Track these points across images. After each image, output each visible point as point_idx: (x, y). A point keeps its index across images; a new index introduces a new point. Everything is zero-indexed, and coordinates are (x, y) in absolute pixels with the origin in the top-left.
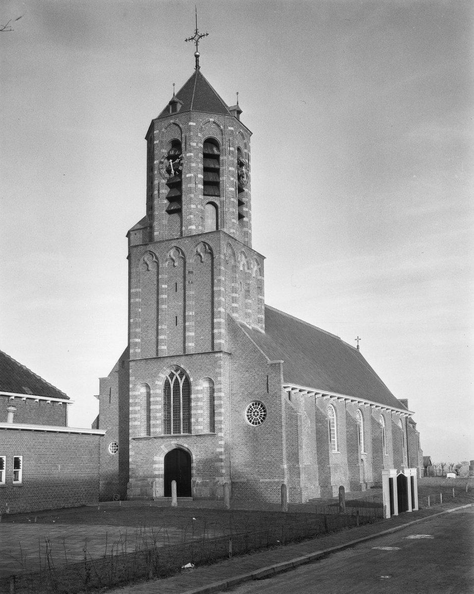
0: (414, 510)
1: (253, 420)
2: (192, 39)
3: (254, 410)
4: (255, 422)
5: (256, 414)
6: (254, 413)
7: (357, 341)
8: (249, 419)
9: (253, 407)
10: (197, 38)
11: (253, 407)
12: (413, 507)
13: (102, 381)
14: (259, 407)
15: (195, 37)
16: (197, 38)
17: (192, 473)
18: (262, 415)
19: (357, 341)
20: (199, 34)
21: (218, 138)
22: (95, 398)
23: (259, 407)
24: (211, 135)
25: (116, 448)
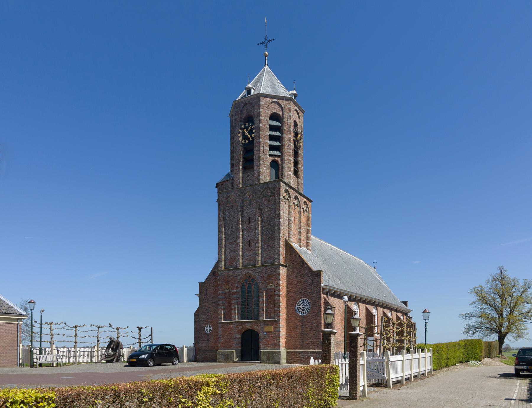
0: (34, 360)
1: (301, 311)
2: (263, 43)
3: (302, 304)
4: (303, 312)
5: (304, 306)
6: (302, 306)
7: (374, 262)
8: (299, 310)
9: (301, 302)
10: (266, 42)
11: (301, 302)
12: (521, 373)
13: (201, 284)
14: (308, 306)
15: (264, 41)
16: (266, 42)
17: (260, 345)
18: (308, 307)
19: (374, 262)
20: (268, 39)
21: (280, 112)
22: (196, 296)
23: (308, 306)
24: (273, 111)
25: (210, 329)
